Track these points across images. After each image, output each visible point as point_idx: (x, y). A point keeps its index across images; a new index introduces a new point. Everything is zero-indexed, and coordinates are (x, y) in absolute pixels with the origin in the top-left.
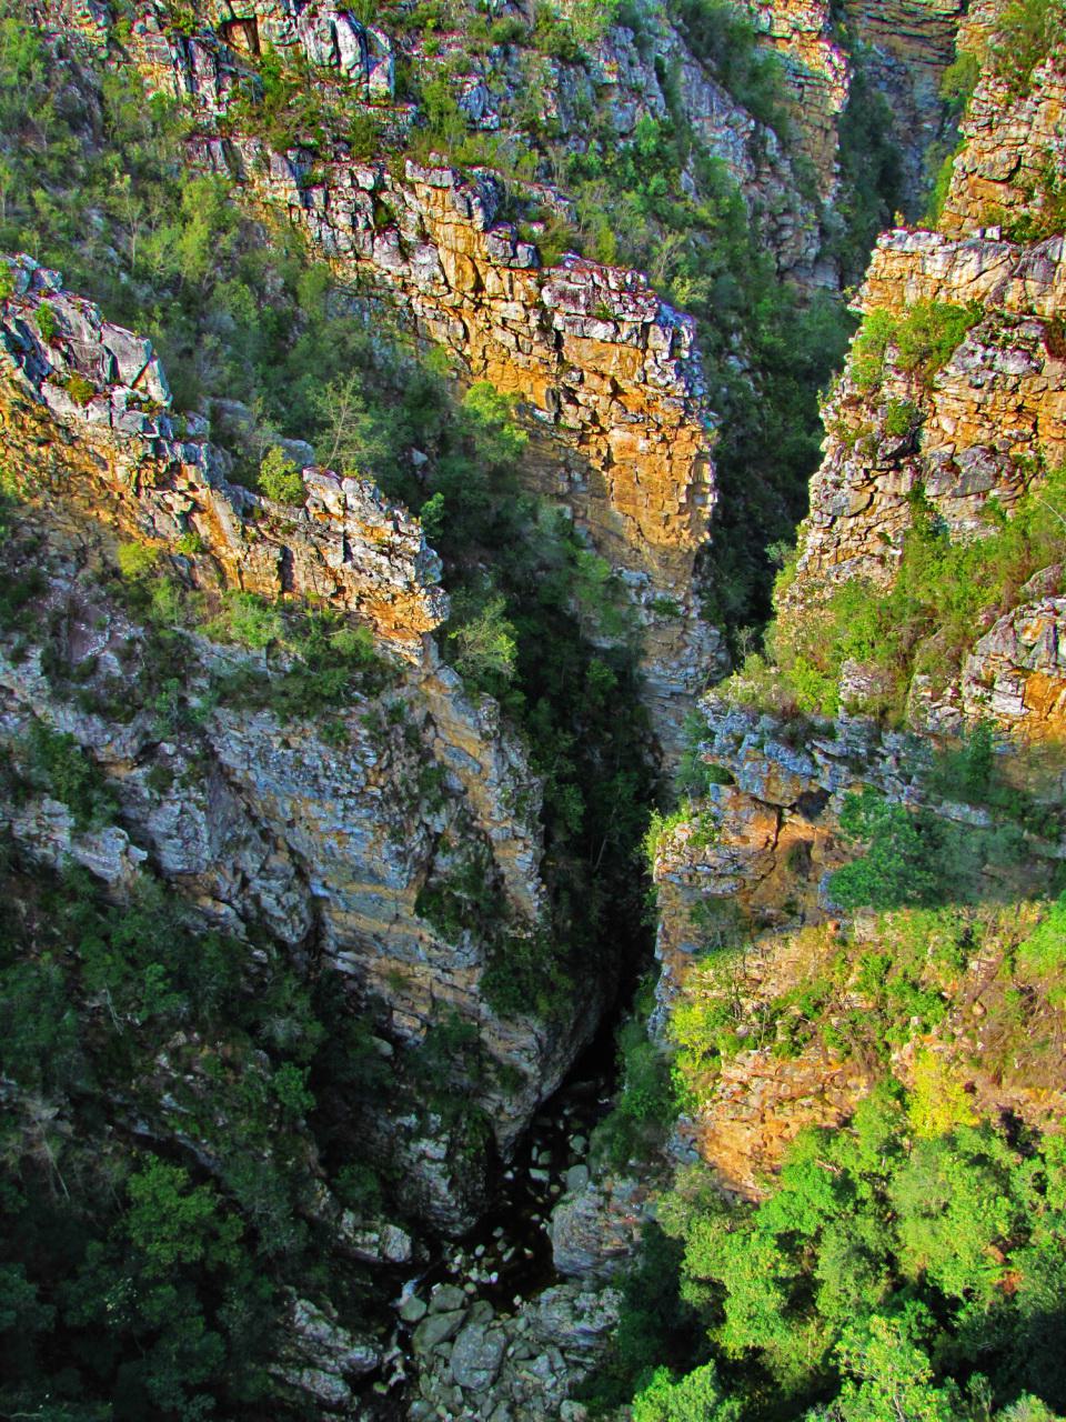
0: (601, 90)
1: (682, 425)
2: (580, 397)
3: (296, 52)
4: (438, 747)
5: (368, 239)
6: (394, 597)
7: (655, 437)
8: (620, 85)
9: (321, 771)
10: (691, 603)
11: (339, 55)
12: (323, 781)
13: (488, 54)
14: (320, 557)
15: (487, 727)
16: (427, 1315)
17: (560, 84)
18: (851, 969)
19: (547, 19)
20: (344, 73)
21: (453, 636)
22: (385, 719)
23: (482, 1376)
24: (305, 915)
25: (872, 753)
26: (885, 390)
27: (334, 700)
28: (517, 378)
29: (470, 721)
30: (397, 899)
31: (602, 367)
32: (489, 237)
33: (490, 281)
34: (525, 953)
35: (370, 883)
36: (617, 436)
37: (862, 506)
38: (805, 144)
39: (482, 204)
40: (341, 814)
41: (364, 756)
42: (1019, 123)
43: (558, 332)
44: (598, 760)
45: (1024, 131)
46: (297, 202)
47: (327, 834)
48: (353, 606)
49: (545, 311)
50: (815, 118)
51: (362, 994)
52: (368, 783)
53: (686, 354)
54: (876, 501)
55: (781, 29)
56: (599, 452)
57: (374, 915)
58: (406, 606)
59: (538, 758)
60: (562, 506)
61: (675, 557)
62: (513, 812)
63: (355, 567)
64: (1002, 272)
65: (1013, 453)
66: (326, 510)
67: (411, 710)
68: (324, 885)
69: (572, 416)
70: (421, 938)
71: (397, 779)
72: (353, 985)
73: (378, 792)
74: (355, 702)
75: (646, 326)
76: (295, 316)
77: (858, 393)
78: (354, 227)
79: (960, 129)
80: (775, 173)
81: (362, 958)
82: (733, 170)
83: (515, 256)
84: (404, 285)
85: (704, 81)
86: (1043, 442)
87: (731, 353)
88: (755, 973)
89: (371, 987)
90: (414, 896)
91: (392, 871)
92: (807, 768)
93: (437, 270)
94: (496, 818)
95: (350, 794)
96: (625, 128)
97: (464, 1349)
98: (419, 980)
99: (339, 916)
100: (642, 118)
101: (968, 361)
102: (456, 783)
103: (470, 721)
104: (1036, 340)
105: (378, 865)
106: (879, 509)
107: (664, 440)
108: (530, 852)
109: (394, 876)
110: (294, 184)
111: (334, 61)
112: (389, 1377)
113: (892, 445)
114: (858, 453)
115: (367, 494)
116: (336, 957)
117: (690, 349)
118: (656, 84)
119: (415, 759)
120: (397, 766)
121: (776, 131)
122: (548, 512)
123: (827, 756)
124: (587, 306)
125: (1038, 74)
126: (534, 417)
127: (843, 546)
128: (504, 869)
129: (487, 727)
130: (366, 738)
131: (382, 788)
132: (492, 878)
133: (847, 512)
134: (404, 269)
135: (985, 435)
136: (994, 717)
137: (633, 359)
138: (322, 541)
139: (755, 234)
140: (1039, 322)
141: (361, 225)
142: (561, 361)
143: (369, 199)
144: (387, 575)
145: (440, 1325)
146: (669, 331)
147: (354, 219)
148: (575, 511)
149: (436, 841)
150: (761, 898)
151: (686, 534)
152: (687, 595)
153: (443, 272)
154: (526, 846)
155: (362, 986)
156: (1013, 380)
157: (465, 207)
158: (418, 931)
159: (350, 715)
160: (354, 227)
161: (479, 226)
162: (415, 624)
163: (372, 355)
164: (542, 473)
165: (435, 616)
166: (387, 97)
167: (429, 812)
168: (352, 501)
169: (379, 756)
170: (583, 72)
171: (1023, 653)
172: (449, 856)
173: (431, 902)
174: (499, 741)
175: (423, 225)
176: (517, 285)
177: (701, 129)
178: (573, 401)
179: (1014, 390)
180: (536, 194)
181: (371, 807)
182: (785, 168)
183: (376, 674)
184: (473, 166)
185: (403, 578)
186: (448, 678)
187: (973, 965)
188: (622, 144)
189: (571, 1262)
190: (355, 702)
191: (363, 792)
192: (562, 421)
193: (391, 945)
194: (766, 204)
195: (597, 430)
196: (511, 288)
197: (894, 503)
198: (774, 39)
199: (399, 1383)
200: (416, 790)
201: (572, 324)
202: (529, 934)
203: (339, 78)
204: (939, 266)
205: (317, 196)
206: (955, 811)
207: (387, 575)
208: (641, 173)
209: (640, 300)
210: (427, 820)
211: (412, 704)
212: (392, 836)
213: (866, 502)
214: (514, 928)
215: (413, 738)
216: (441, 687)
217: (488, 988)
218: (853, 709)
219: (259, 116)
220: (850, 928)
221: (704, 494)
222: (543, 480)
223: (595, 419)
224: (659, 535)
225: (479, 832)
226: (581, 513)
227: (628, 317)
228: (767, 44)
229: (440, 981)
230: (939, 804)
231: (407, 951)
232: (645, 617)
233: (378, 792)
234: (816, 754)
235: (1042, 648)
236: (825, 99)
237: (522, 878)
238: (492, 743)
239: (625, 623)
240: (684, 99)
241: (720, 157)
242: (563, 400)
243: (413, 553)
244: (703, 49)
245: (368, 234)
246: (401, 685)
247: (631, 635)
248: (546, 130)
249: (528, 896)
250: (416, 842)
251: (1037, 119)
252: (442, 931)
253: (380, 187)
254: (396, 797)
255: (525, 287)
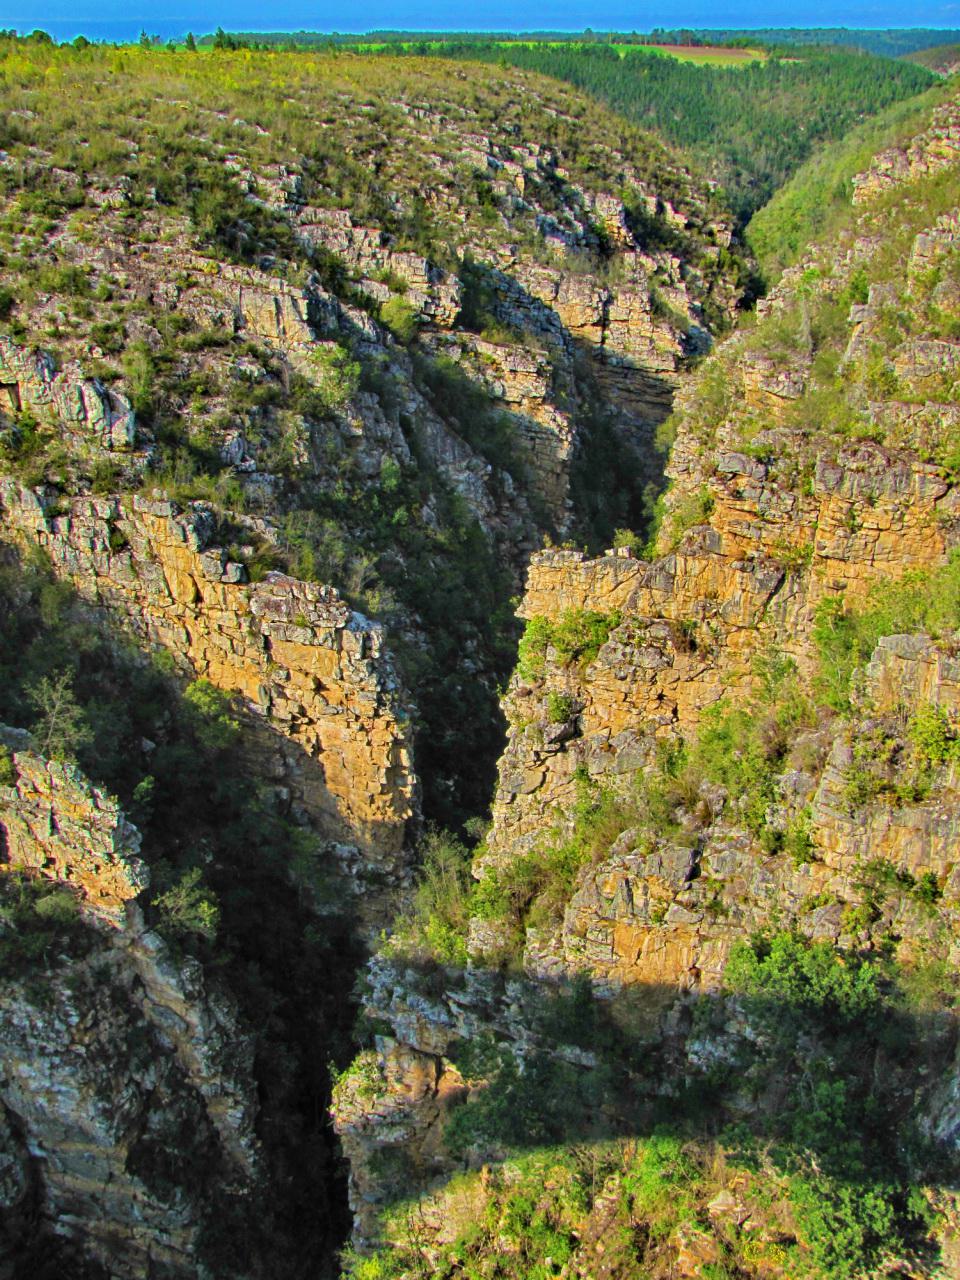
0: (350, 441)
1: (377, 715)
2: (288, 692)
3: (51, 409)
4: (147, 1006)
5: (105, 559)
6: (98, 868)
7: (355, 726)
8: (367, 438)
9: (28, 1031)
10: (402, 873)
11: (86, 412)
12: (32, 1041)
13: (248, 412)
14: (30, 831)
15: (190, 988)
17: (312, 436)
18: (501, 1212)
19: (302, 386)
20: (90, 426)
21: (156, 903)
22: (90, 981)
24: (20, 1177)
25: (499, 1002)
26: (549, 683)
27: (38, 961)
28: (235, 675)
29: (173, 981)
30: (108, 1157)
31: (305, 666)
32: (203, 556)
33: (206, 593)
34: (239, 1210)
36: (323, 726)
37: (538, 784)
38: (539, 485)
39: (196, 529)
40: (47, 1072)
41: (68, 1015)
43: (266, 637)
44: (321, 1021)
46: (44, 527)
47: (36, 1092)
48: (63, 876)
49: (253, 619)
50: (547, 464)
51: (80, 1260)
52: (73, 1042)
53: (377, 655)
54: (548, 779)
55: (512, 395)
56: (308, 740)
57: (88, 1174)
58: (110, 875)
59: (248, 1017)
60: (278, 788)
61: (383, 832)
62: (220, 1069)
63: (61, 839)
64: (634, 583)
65: (659, 734)
66: (36, 790)
67: (119, 972)
68: (40, 1146)
69: (283, 710)
70: (135, 1197)
71: (104, 1038)
72: (69, 1250)
73: (82, 1050)
74: (62, 964)
75: (338, 631)
76: (38, 623)
77: (528, 687)
78: (93, 548)
79: (666, 473)
80: (514, 508)
81: (82, 1221)
82: (475, 504)
83: (225, 572)
84: (137, 597)
85: (447, 434)
86: (682, 724)
87: (466, 657)
88: (432, 1221)
89: (89, 1250)
90: (124, 1153)
91: (98, 1128)
92: (444, 1018)
93: (162, 584)
94: (204, 1074)
95: (56, 1053)
96: (371, 471)
98: (139, 1242)
99: (57, 1178)
100: (388, 463)
101: (611, 656)
102: (166, 1041)
103: (173, 981)
104: (665, 639)
105: (86, 1123)
106: (552, 786)
107: (362, 728)
108: (241, 1108)
109: (101, 1134)
110: (41, 513)
111: (81, 416)
113: (557, 729)
114: (528, 737)
115: (69, 774)
116: (56, 1221)
117: (380, 650)
118: (402, 437)
119: (123, 1018)
120: (104, 1025)
121: (510, 472)
122: (265, 792)
123: (460, 1005)
124: (288, 614)
125: (720, 433)
126: (249, 709)
127: (525, 819)
128: (218, 1125)
129: (190, 988)
130: (69, 998)
131: (87, 1046)
132: (206, 1134)
133: (525, 788)
134: (136, 583)
135: (634, 720)
136: (592, 964)
137: (331, 660)
138: (31, 817)
139: (499, 559)
140: (666, 624)
141: (99, 547)
142: (270, 659)
143: (106, 526)
144: (89, 846)
146: (360, 635)
147: (93, 543)
148: (292, 792)
149: (149, 1099)
150: (428, 1145)
151: (390, 811)
152: (396, 867)
153: (168, 586)
154: (237, 1103)
155: (80, 1251)
156: (650, 673)
157: (180, 532)
158: (131, 1191)
159: (56, 976)
160: (93, 548)
161: (194, 548)
162: (119, 891)
163: (111, 657)
164: (261, 759)
165: (134, 884)
166: (127, 444)
167: (138, 1070)
168: (56, 781)
169: (83, 1016)
170: (333, 426)
171: (605, 904)
172: (160, 1112)
173: (143, 1161)
174: (205, 1001)
175: (151, 548)
176: (230, 597)
177: (447, 471)
178: (282, 695)
179: (653, 681)
180: (248, 521)
181: (74, 1065)
182: (522, 503)
183: (82, 936)
184: (195, 499)
185: (103, 849)
186: (152, 942)
187: (598, 1202)
188: (369, 483)
190: (62, 964)
191: (68, 1051)
192: (274, 712)
193: (108, 1205)
194: (506, 532)
195: (306, 720)
196: (225, 600)
197: (565, 780)
198: (508, 403)
200: (124, 1048)
201: (277, 629)
202: (246, 1191)
203: (86, 430)
204: (582, 579)
205: (62, 522)
206: (569, 1052)
207: (89, 846)
208: (386, 507)
209: (332, 609)
210: (137, 1077)
211: (119, 965)
212: (99, 1092)
213: (540, 779)
214: (230, 1184)
215: (122, 999)
216: (146, 951)
217: (204, 1246)
218: (480, 962)
219: (15, 459)
220: (500, 1171)
221: (404, 776)
222: (262, 765)
223: (303, 712)
224: (370, 813)
225: (190, 1088)
226: (298, 794)
227: (322, 624)
228: (502, 407)
229: (158, 1242)
230: (554, 1047)
231: (124, 1205)
232: (357, 887)
233: (82, 1050)
234: (451, 1003)
235: (619, 899)
236: (554, 450)
237: (235, 1135)
238: (197, 1002)
239: (340, 891)
240: (431, 449)
241: (463, 495)
242: (274, 695)
243: (112, 827)
244: (447, 410)
245: (105, 554)
246: (109, 949)
247: (346, 903)
248: (298, 472)
249: (243, 1151)
250: (125, 1098)
252: (152, 1189)
253: (117, 516)
254: (102, 1054)
255: (236, 598)
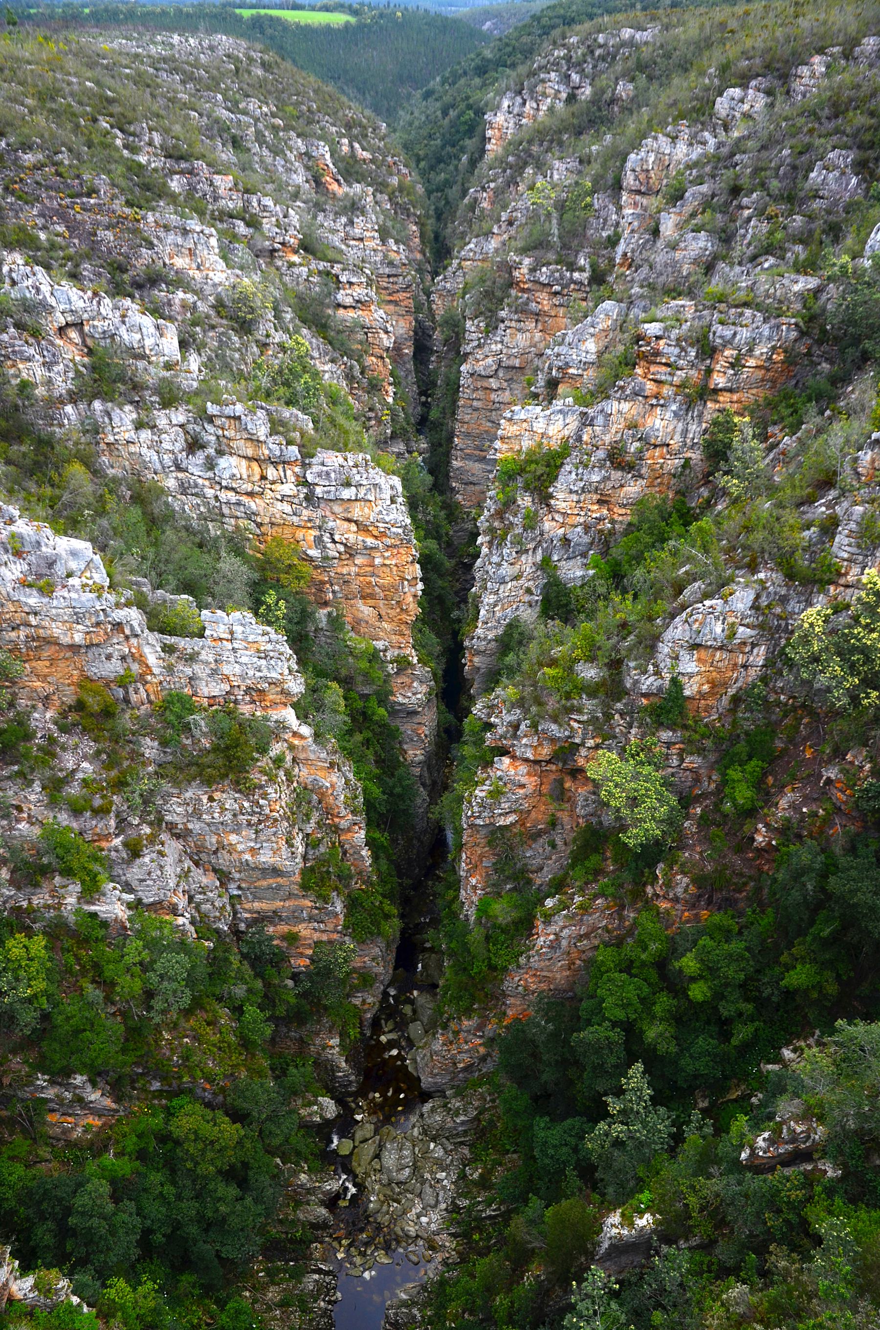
16: (355, 1147)
23: (407, 1172)
35: (272, 877)
42: (496, 342)
45: (499, 346)
97: (390, 1159)
112: (346, 1195)
145: (369, 1149)
176: (289, 473)
177: (315, 365)
189: (435, 1083)
199: (353, 1195)
204: (541, 425)
222: (315, 595)
234: (572, 723)
251: (505, 339)
